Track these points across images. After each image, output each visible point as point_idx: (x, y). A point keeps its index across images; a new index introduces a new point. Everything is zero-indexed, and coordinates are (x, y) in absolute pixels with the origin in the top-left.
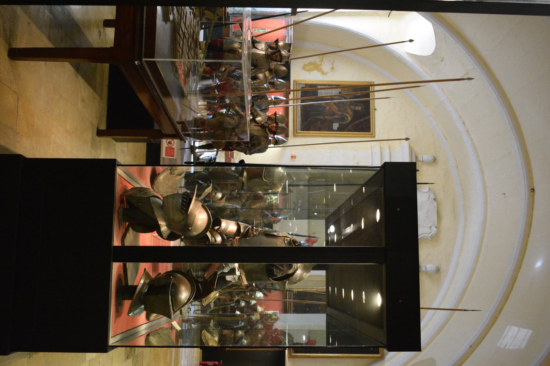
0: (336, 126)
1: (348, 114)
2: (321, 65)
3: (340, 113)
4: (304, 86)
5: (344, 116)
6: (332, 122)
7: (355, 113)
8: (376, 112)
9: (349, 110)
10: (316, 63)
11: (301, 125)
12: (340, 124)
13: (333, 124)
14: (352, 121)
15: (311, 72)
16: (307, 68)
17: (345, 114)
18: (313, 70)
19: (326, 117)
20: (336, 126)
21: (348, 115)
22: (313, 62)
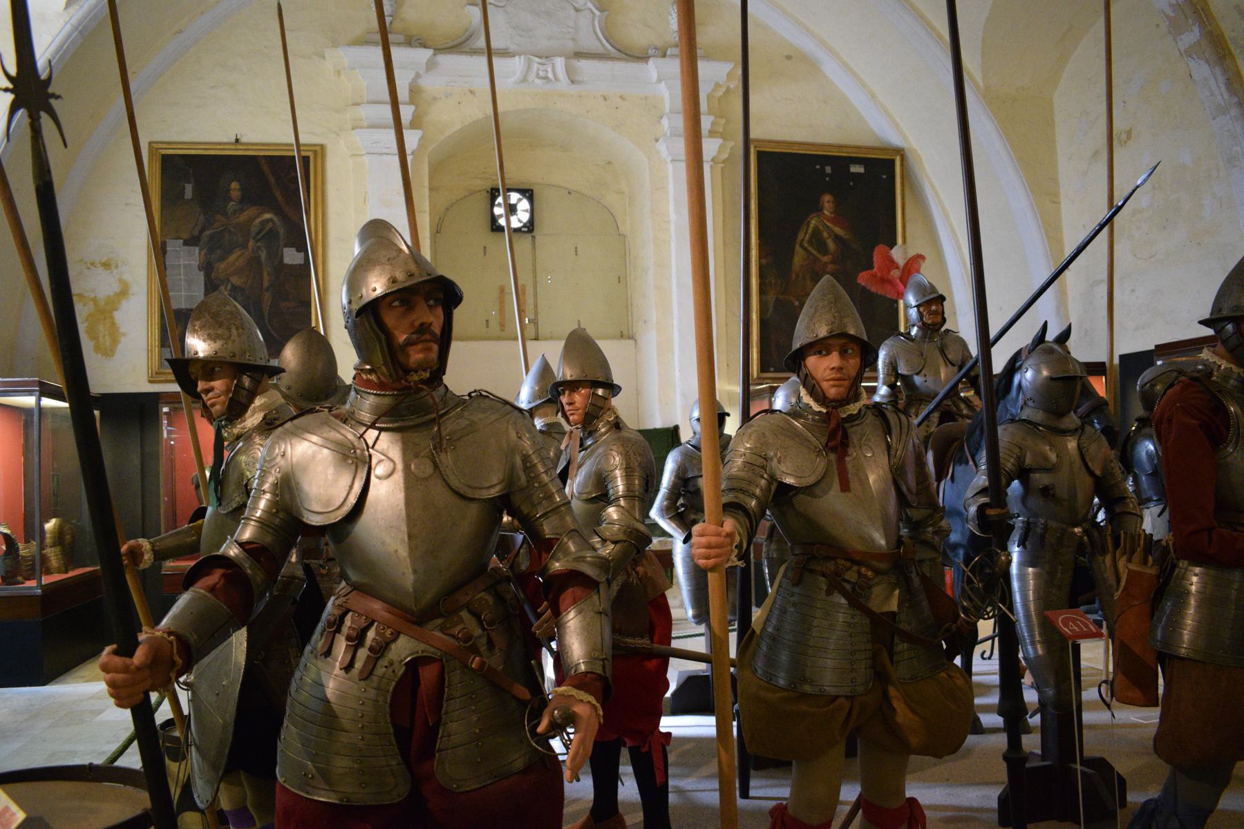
0: (291, 257)
1: (251, 220)
2: (95, 300)
3: (251, 243)
6: (280, 268)
7: (247, 199)
8: (244, 140)
9: (243, 217)
13: (287, 265)
14: (278, 211)
15: (122, 330)
17: (254, 229)
18: (113, 324)
19: (266, 284)
20: (291, 257)
21: (258, 221)
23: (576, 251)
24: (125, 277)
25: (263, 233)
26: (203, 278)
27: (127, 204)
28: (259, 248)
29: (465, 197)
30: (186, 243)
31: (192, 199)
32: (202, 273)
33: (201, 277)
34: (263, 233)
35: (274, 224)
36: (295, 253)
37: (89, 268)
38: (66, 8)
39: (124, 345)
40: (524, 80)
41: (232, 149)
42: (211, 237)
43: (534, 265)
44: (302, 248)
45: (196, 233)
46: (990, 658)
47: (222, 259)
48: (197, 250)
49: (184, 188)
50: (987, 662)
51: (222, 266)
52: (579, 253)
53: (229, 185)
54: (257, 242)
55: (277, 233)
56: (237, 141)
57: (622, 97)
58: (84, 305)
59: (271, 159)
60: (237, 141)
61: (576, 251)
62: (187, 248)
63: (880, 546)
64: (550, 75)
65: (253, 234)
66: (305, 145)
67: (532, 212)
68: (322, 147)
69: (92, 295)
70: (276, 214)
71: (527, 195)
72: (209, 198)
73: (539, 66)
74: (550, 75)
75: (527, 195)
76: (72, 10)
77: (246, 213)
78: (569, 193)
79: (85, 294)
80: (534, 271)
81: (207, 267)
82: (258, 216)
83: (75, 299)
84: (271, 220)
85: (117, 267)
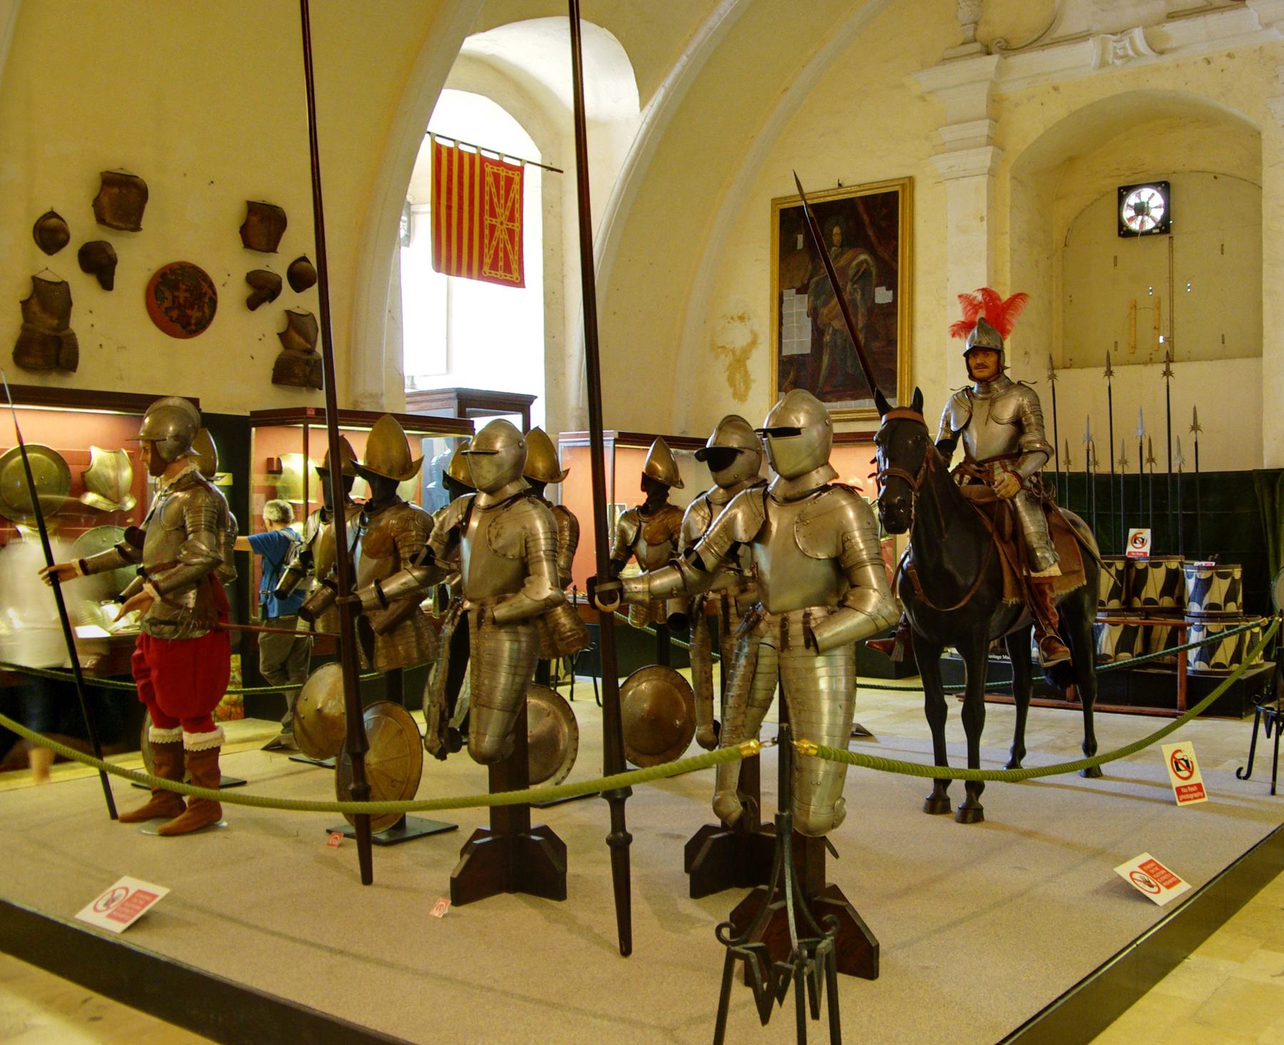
0: (882, 296)
2: (733, 351)
5: (857, 272)
9: (842, 262)
13: (879, 305)
14: (872, 251)
15: (752, 377)
16: (742, 390)
17: (851, 272)
18: (746, 371)
20: (882, 296)
21: (855, 263)
22: (727, 373)
23: (1222, 250)
25: (860, 273)
26: (810, 324)
27: (756, 260)
28: (854, 289)
30: (799, 291)
32: (810, 319)
33: (808, 323)
34: (860, 273)
35: (868, 264)
36: (885, 291)
37: (729, 322)
38: (641, 110)
40: (1103, 64)
41: (883, 187)
42: (817, 284)
43: (1171, 271)
44: (892, 285)
46: (1246, 778)
50: (1242, 782)
51: (825, 311)
52: (1225, 252)
53: (832, 231)
54: (853, 284)
55: (871, 274)
57: (1230, 56)
58: (726, 356)
59: (865, 199)
60: (840, 185)
61: (1222, 250)
64: (1130, 52)
65: (850, 278)
66: (810, 196)
67: (1167, 207)
68: (911, 179)
69: (731, 347)
71: (1125, 193)
72: (817, 249)
73: (1115, 44)
74: (1130, 52)
75: (1125, 193)
77: (845, 256)
78: (1215, 177)
79: (727, 346)
80: (1171, 281)
81: (814, 313)
82: (854, 259)
84: (865, 261)
85: (749, 319)
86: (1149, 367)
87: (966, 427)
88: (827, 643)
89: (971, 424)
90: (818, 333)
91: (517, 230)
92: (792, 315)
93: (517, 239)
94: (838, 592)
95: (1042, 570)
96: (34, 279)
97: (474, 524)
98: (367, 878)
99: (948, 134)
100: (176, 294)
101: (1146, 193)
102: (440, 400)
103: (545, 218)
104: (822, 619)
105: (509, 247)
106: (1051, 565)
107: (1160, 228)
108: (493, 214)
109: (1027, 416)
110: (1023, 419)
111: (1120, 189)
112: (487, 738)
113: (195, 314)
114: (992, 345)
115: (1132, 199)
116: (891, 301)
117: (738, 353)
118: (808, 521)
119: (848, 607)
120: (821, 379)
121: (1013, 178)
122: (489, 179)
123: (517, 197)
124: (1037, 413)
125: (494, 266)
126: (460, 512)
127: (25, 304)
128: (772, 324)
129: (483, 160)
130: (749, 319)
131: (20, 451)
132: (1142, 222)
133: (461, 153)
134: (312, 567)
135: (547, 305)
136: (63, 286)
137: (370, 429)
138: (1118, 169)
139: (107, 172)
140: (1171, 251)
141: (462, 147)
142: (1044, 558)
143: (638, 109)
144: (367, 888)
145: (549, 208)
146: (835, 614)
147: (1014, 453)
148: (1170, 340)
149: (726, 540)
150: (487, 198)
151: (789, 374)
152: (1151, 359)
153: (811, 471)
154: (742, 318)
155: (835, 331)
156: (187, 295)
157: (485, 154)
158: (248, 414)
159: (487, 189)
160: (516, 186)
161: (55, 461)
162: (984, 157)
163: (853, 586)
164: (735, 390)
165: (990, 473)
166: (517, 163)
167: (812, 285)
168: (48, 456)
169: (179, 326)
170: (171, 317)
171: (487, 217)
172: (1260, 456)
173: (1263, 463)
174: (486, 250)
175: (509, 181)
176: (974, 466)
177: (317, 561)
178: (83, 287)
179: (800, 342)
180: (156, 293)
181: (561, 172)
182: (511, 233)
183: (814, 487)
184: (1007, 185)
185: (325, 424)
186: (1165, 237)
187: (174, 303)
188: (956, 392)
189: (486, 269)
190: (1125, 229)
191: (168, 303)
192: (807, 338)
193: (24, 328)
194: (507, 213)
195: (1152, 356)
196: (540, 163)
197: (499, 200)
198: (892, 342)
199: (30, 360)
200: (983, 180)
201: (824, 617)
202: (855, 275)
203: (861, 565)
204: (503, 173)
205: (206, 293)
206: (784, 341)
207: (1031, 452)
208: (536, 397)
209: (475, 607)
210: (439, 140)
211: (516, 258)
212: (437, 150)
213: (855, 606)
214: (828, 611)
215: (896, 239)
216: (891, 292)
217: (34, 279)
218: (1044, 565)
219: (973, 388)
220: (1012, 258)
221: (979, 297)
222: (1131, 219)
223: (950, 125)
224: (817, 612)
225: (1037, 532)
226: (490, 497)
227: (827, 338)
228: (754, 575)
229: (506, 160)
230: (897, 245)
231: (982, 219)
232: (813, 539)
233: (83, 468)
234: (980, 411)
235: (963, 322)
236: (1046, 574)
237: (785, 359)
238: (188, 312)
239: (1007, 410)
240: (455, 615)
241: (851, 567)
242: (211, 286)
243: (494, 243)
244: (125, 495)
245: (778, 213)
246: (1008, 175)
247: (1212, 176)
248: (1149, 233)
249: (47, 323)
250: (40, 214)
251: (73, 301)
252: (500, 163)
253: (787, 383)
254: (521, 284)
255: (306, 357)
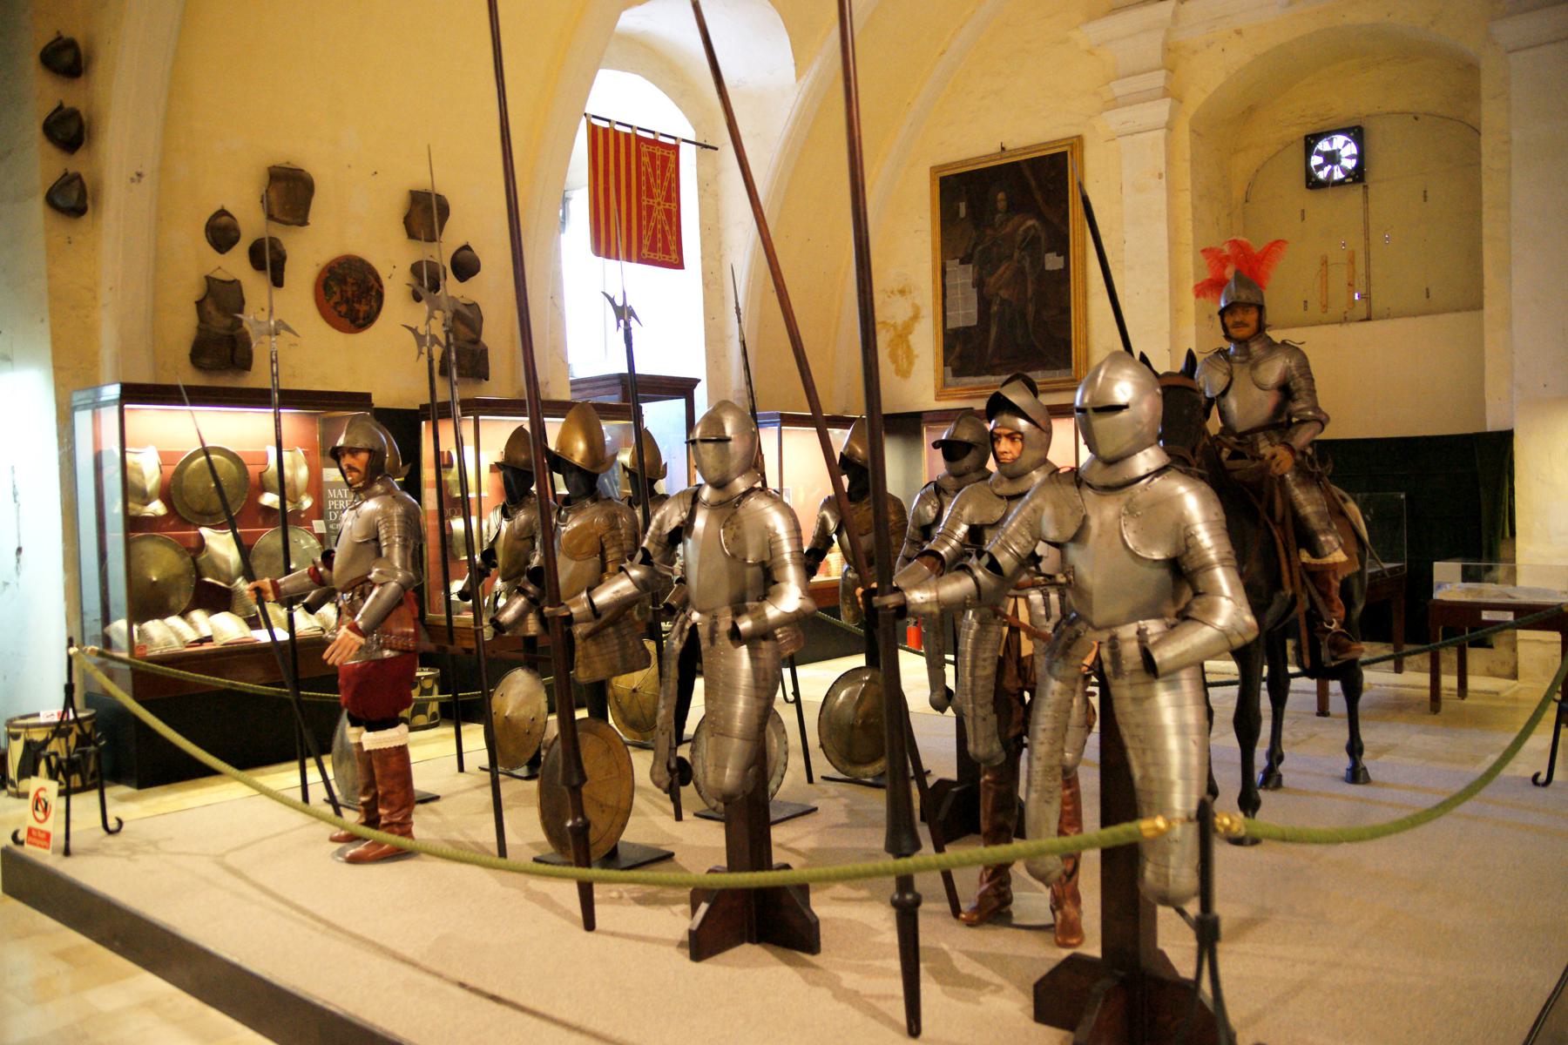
0: (1053, 262)
1: (1015, 230)
2: (894, 326)
3: (1016, 254)
4: (949, 369)
5: (1025, 239)
7: (1014, 208)
8: (1009, 147)
10: (892, 341)
11: (1058, 368)
12: (1049, 250)
13: (1048, 271)
14: (1040, 216)
15: (916, 352)
16: (905, 366)
17: (1019, 239)
18: (909, 347)
20: (1053, 262)
21: (1022, 229)
22: (889, 350)
23: (1425, 197)
24: (916, 301)
29: (1279, 151)
30: (962, 262)
31: (965, 218)
32: (975, 290)
38: (797, 80)
39: (918, 364)
45: (969, 251)
47: (992, 274)
48: (970, 267)
49: (959, 207)
51: (992, 280)
56: (1003, 149)
58: (887, 331)
60: (1003, 149)
61: (1425, 197)
62: (962, 266)
63: (524, 603)
67: (1360, 157)
68: (1080, 138)
70: (1038, 219)
72: (980, 215)
76: (802, 81)
78: (1416, 118)
81: (979, 284)
83: (878, 327)
84: (1033, 226)
86: (1345, 326)
87: (1224, 393)
88: (1168, 666)
89: (1231, 392)
90: (984, 304)
91: (674, 210)
92: (955, 287)
93: (674, 219)
94: (1176, 598)
95: (1326, 556)
96: (208, 278)
97: (700, 522)
98: (589, 924)
99: (1119, 88)
100: (344, 288)
101: (1339, 140)
102: (604, 387)
103: (701, 197)
104: (1161, 635)
105: (667, 228)
106: (1335, 550)
107: (1353, 177)
108: (650, 195)
109: (1296, 381)
110: (1291, 384)
111: (1306, 137)
112: (728, 772)
113: (363, 308)
114: (1253, 299)
115: (1323, 146)
116: (1062, 267)
117: (900, 328)
118: (1139, 513)
119: (1194, 619)
120: (990, 351)
121: (1193, 131)
122: (645, 159)
123: (673, 176)
124: (1308, 376)
125: (653, 248)
126: (682, 509)
127: (200, 304)
128: (935, 296)
129: (639, 139)
130: (910, 292)
131: (202, 453)
132: (1331, 172)
133: (617, 133)
134: (495, 565)
135: (706, 285)
136: (235, 285)
137: (563, 420)
138: (1303, 116)
139: (274, 167)
140: (1366, 200)
141: (618, 127)
142: (1327, 541)
143: (794, 79)
144: (590, 935)
145: (708, 188)
146: (1176, 629)
147: (1280, 423)
148: (1366, 297)
149: (1030, 539)
150: (644, 178)
151: (954, 347)
152: (1345, 318)
153: (1135, 454)
154: (902, 292)
155: (1003, 301)
156: (355, 288)
157: (640, 133)
158: (418, 408)
159: (643, 169)
160: (672, 166)
161: (233, 462)
162: (1160, 110)
163: (1197, 594)
164: (897, 366)
165: (1253, 445)
166: (672, 142)
167: (977, 254)
168: (226, 457)
169: (348, 321)
170: (340, 312)
171: (644, 198)
172: (1483, 420)
173: (1485, 425)
174: (644, 232)
175: (665, 160)
176: (1233, 439)
177: (500, 559)
178: (255, 285)
179: (966, 314)
180: (325, 289)
181: (716, 149)
182: (668, 212)
183: (1142, 472)
184: (1184, 136)
185: (525, 415)
186: (1360, 187)
187: (342, 297)
188: (1207, 356)
189: (645, 251)
190: (1313, 180)
191: (336, 298)
192: (973, 310)
193: (199, 329)
194: (664, 193)
195: (1347, 315)
196: (693, 140)
197: (655, 180)
198: (1066, 311)
199: (206, 361)
200: (1161, 134)
201: (1163, 632)
202: (1023, 242)
203: (1207, 567)
204: (658, 152)
205: (372, 287)
206: (948, 314)
207: (1302, 422)
208: (699, 381)
209: (707, 619)
210: (595, 122)
211: (674, 238)
212: (593, 130)
213: (1203, 618)
214: (1167, 625)
215: (1067, 201)
216: (1061, 259)
217: (208, 278)
218: (1327, 549)
219: (1229, 349)
220: (1194, 216)
221: (1227, 250)
222: (1320, 168)
223: (1123, 77)
224: (1153, 627)
225: (1315, 512)
226: (715, 491)
227: (995, 308)
228: (1069, 582)
229: (662, 139)
230: (1068, 208)
231: (1160, 176)
232: (1149, 538)
233: (259, 468)
234: (1241, 376)
235: (1210, 280)
236: (1330, 560)
237: (950, 333)
238: (357, 306)
239: (1274, 370)
240: (682, 629)
241: (1195, 571)
242: (378, 279)
243: (652, 224)
244: (302, 494)
245: (938, 182)
246: (1187, 128)
247: (1411, 118)
248: (1341, 182)
249: (219, 323)
250: (211, 213)
251: (246, 296)
252: (655, 142)
253: (952, 358)
254: (679, 265)
255: (470, 347)
